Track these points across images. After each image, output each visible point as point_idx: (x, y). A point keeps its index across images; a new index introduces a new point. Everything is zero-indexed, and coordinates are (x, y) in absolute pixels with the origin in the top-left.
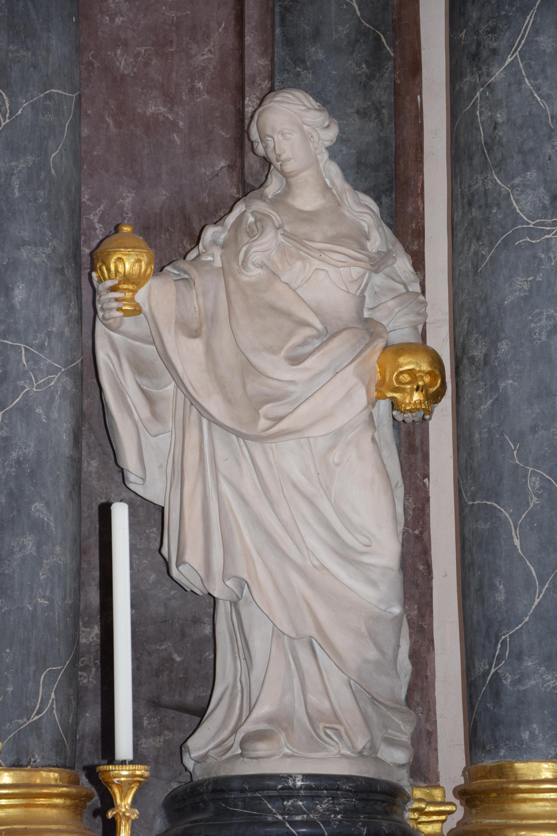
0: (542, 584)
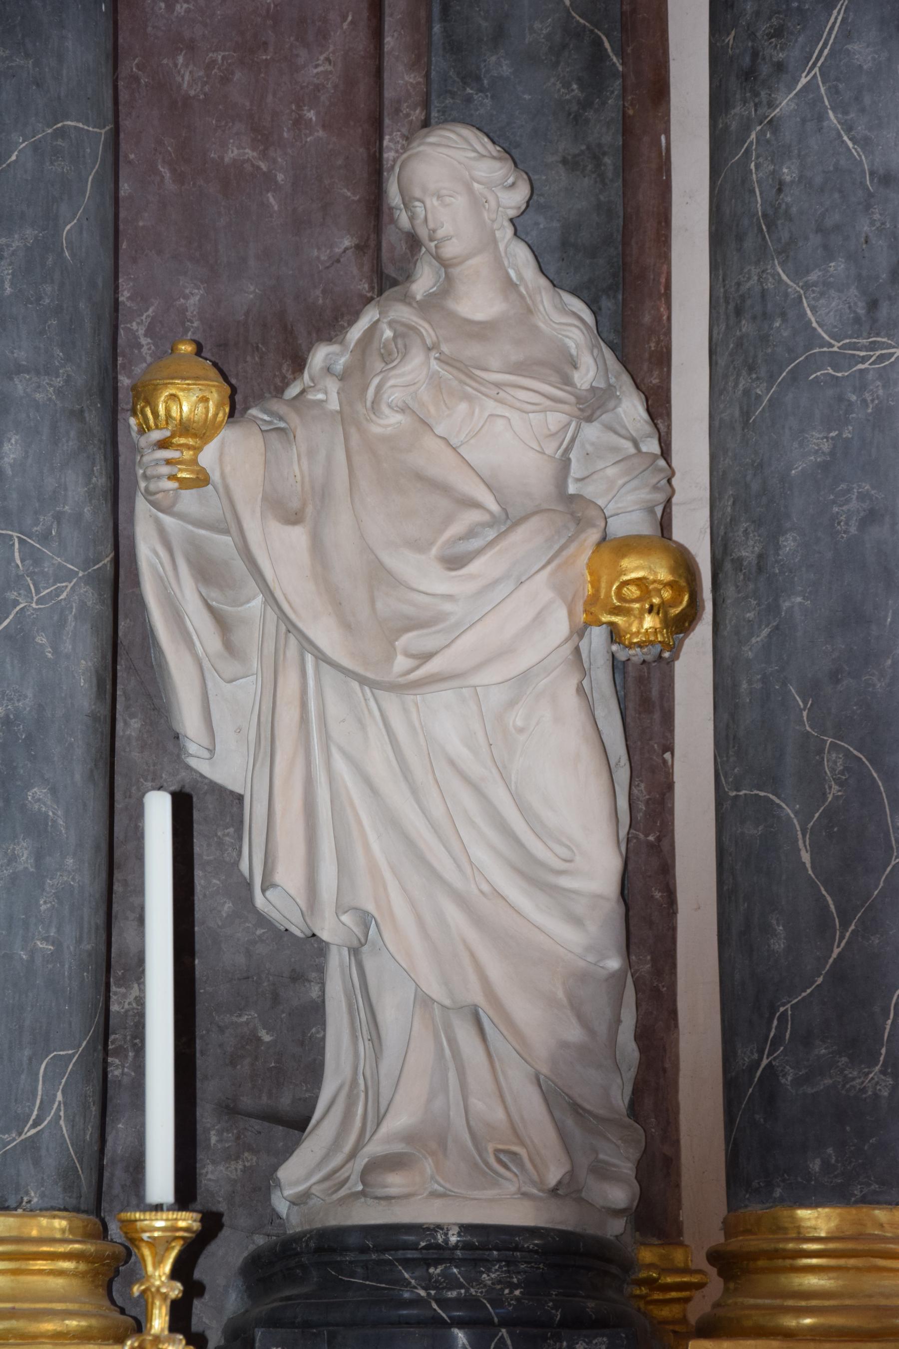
0: (845, 925)
